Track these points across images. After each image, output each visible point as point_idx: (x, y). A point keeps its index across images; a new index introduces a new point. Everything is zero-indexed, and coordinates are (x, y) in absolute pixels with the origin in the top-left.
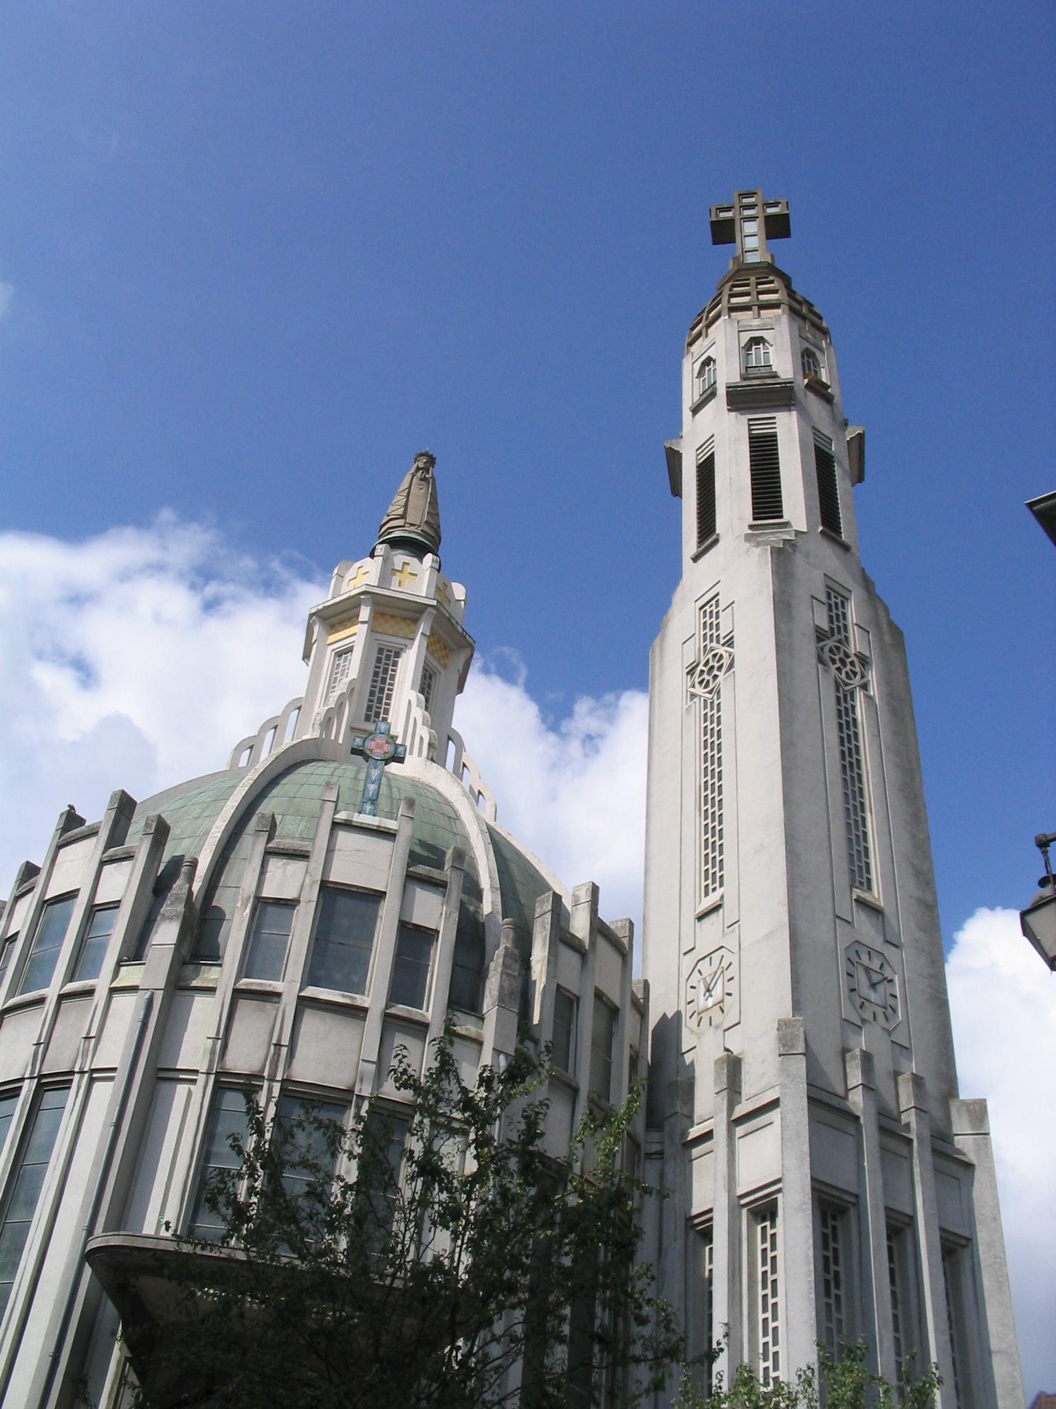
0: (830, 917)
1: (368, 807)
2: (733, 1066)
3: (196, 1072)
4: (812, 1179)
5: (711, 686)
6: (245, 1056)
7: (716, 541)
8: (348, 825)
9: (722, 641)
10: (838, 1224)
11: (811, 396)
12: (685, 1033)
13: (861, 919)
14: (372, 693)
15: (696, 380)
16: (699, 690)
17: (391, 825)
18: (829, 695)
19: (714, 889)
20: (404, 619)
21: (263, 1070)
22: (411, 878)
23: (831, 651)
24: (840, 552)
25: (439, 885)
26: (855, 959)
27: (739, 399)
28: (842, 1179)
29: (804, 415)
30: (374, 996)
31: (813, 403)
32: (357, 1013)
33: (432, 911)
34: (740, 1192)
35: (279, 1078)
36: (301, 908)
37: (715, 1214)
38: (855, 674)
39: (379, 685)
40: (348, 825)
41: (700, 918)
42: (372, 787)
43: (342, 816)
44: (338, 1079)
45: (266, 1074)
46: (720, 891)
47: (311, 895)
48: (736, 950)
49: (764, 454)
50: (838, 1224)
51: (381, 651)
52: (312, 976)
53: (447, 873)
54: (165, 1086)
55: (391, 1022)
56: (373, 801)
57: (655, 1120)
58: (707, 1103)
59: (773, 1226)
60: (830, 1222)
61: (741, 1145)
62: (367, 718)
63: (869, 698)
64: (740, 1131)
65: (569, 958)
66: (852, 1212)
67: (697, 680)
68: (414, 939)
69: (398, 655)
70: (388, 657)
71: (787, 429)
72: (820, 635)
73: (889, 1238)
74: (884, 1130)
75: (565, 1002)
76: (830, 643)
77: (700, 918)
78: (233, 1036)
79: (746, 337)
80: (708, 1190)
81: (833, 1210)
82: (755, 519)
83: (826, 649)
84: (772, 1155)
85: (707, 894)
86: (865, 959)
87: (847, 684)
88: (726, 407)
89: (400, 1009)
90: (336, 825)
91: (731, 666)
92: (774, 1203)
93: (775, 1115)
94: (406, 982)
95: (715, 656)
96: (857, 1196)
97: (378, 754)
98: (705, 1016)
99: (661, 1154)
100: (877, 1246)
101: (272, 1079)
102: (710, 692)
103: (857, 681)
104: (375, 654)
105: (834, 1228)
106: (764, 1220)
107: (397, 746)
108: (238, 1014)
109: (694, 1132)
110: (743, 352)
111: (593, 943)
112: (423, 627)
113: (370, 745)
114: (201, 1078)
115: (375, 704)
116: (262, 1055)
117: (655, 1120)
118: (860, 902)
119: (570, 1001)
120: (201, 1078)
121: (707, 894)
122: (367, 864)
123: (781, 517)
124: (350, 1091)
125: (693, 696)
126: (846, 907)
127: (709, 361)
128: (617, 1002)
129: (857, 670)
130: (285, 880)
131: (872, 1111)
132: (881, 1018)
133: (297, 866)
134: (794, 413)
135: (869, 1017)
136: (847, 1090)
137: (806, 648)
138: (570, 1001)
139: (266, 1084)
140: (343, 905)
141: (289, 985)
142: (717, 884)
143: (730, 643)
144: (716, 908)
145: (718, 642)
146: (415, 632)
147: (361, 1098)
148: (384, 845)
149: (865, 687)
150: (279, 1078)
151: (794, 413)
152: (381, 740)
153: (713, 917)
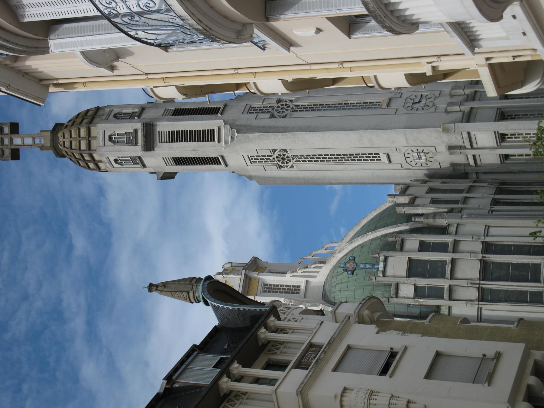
0: (396, 116)
1: (376, 266)
2: (451, 148)
3: (478, 308)
4: (495, 121)
5: (291, 159)
6: (474, 294)
7: (223, 157)
8: (384, 272)
9: (272, 154)
10: (506, 114)
11: (143, 116)
12: (433, 167)
13: (394, 105)
14: (285, 293)
15: (124, 166)
16: (290, 164)
17: (382, 258)
18: (296, 114)
19: (379, 157)
20: (249, 283)
21: (476, 287)
22: (401, 250)
23: (279, 112)
24: (227, 109)
25: (403, 241)
26: (410, 108)
27: (149, 146)
28: (493, 113)
29: (158, 119)
30: (446, 257)
31: (148, 115)
32: (453, 262)
33: (413, 242)
34: (495, 145)
35: (479, 282)
36: (416, 283)
37: (501, 153)
38: (286, 105)
39: (281, 291)
40: (384, 272)
41: (390, 161)
42: (368, 266)
43: (380, 274)
44: (477, 265)
45: (478, 286)
46: (381, 155)
47: (413, 280)
48: (407, 148)
49: (176, 137)
50: (506, 114)
51: (265, 291)
52: (443, 276)
53: (399, 239)
54: (483, 318)
55: (455, 250)
56: (373, 265)
57: (465, 175)
58: (459, 158)
59: (508, 135)
60: (506, 117)
61: (480, 145)
62: (298, 293)
63: (297, 99)
64: (475, 146)
65: (417, 202)
66: (503, 110)
67: (286, 165)
68: (424, 247)
69: (266, 285)
70: (267, 288)
71: (165, 126)
72: (272, 116)
73: (508, 99)
74: (473, 99)
75: (434, 202)
76: (275, 113)
77: (390, 161)
78: (465, 299)
79: (108, 143)
80: (490, 158)
81: (503, 116)
82: (214, 140)
83: (279, 114)
84: (484, 135)
85: (380, 160)
86: (408, 105)
87: (293, 108)
88: (152, 152)
89: (450, 247)
90: (384, 276)
91: (286, 151)
92: (501, 134)
93: (472, 134)
94: (442, 248)
95: (277, 157)
96: (498, 109)
97: (354, 266)
98: (429, 159)
99: (477, 173)
100: (510, 103)
101: (479, 284)
102: (293, 159)
103: (289, 104)
104: (267, 293)
105: (508, 116)
106: (505, 138)
107: (350, 260)
108: (458, 298)
109: (472, 162)
110: (117, 144)
111: (408, 195)
112: (255, 275)
113: (350, 268)
114: (480, 306)
115: (291, 291)
116: (471, 289)
117: (465, 175)
118: (388, 105)
119: (433, 201)
120: (480, 306)
121: (380, 160)
122: (397, 265)
123: (214, 130)
124: (481, 260)
125: (292, 166)
126: (391, 111)
127: (116, 161)
128: (427, 188)
129: (284, 103)
130: (407, 290)
131: (467, 103)
132: (431, 100)
133: (401, 286)
134: (158, 123)
135: (431, 104)
136: (460, 111)
137: (279, 122)
138: (433, 201)
139: (481, 286)
140: (414, 269)
141: (445, 283)
142: (378, 156)
143: (274, 151)
144: (388, 156)
145: (271, 156)
146: (255, 279)
147: (483, 257)
148: (390, 260)
149: (291, 101)
150: (479, 282)
151: (158, 123)
152: (348, 265)
153: (391, 157)
